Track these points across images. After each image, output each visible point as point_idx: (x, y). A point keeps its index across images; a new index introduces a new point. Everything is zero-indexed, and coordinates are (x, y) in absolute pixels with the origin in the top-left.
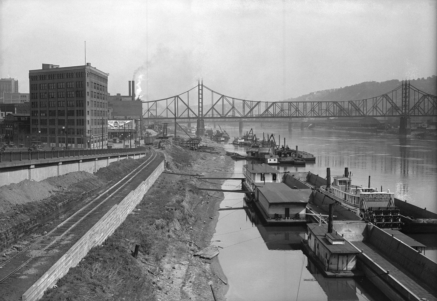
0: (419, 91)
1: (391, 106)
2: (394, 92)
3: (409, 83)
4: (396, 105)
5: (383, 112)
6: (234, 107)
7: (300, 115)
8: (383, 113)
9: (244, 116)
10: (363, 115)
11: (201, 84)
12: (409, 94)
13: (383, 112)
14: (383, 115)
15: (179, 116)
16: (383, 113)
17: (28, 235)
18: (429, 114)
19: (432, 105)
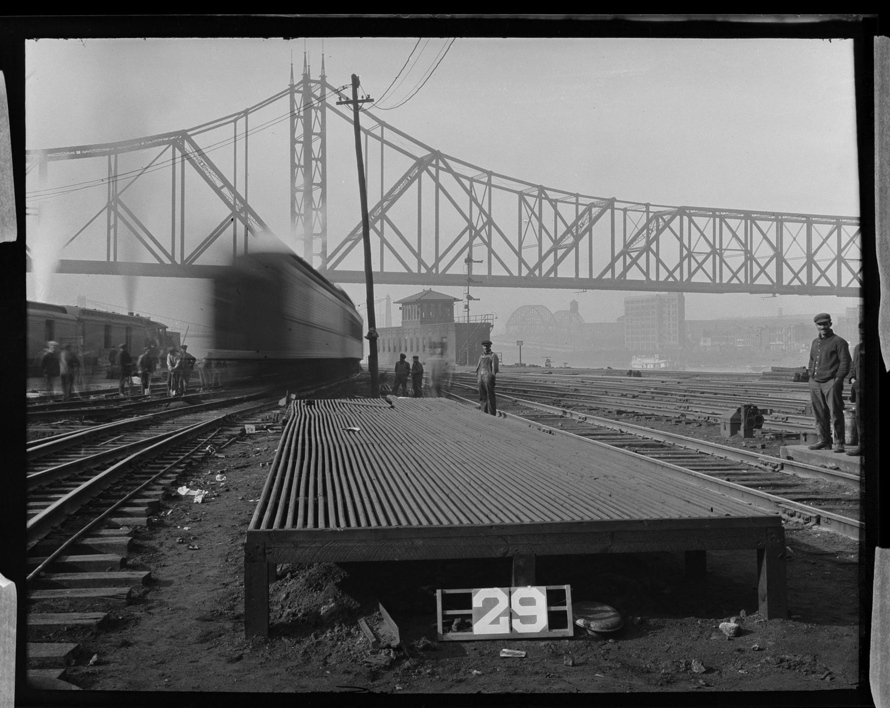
0: (388, 135)
1: (466, 224)
2: (241, 122)
3: (323, 77)
4: (244, 202)
5: (418, 255)
6: (247, 209)
7: (498, 271)
8: (421, 262)
9: (178, 260)
10: (415, 270)
11: (315, 76)
12: (323, 146)
13: (418, 255)
14: (525, 272)
15: (725, 281)
16: (421, 262)
17: (326, 586)
18: (543, 273)
19: (466, 224)
